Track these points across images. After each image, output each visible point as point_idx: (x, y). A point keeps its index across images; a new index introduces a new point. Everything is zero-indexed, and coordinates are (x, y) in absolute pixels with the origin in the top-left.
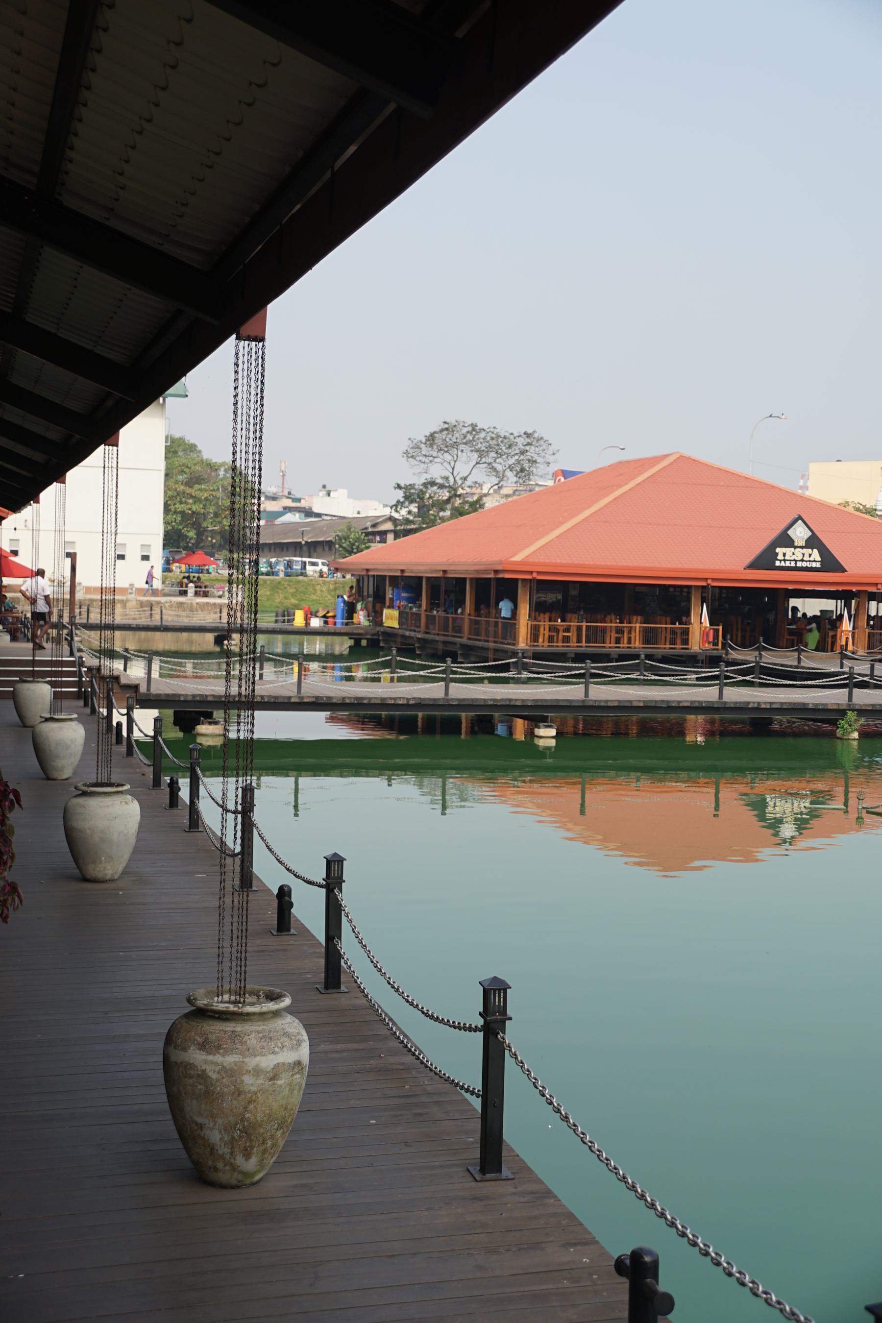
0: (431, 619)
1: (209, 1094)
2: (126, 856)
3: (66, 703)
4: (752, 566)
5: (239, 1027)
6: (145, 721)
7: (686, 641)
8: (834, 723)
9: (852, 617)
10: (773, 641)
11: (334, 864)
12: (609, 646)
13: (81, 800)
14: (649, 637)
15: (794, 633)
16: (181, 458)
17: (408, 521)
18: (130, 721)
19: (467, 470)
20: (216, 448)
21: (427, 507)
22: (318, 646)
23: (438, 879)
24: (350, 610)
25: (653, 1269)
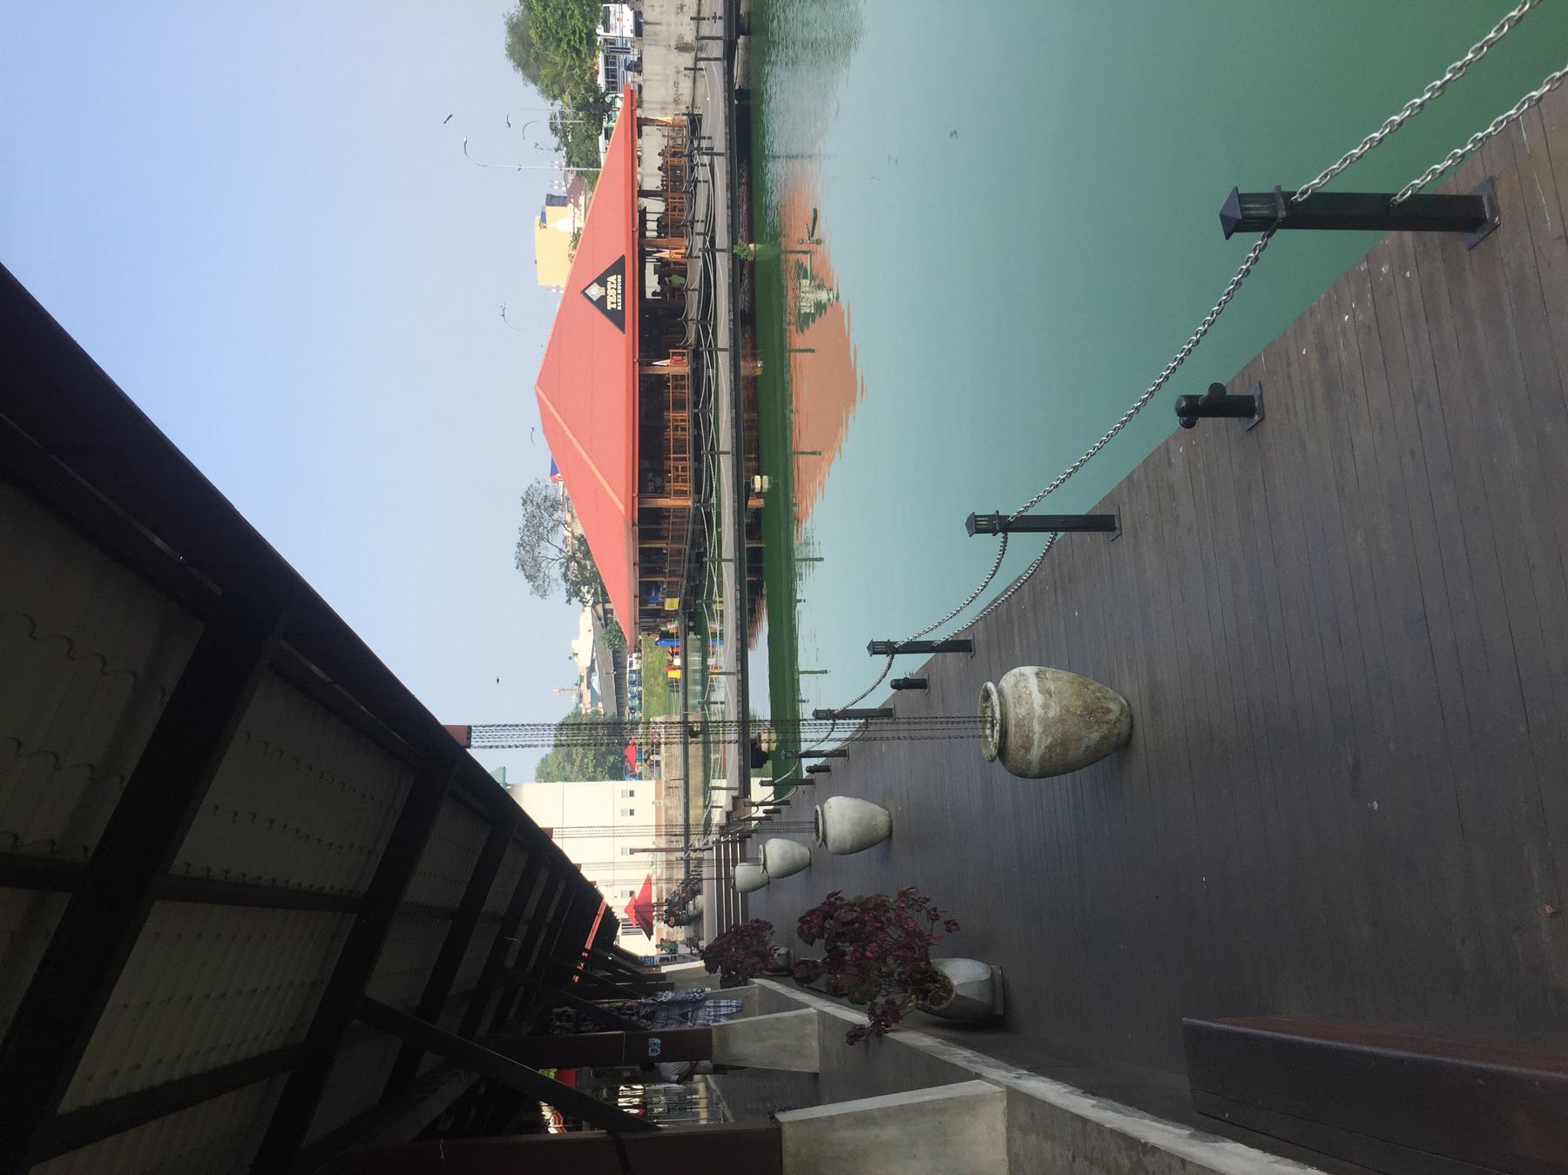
0: (672, 573)
1: (1062, 744)
2: (871, 805)
3: (749, 854)
4: (622, 328)
5: (1012, 722)
6: (761, 792)
7: (683, 377)
8: (742, 263)
9: (659, 249)
10: (680, 310)
11: (876, 648)
12: (688, 436)
13: (830, 843)
14: (680, 405)
15: (673, 295)
16: (553, 768)
17: (595, 594)
18: (763, 803)
19: (553, 550)
20: (544, 750)
21: (584, 578)
22: (694, 659)
23: (877, 568)
24: (666, 636)
25: (1191, 399)
